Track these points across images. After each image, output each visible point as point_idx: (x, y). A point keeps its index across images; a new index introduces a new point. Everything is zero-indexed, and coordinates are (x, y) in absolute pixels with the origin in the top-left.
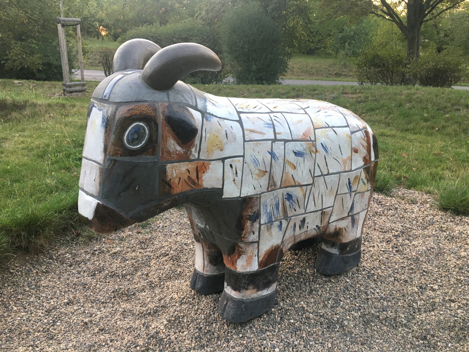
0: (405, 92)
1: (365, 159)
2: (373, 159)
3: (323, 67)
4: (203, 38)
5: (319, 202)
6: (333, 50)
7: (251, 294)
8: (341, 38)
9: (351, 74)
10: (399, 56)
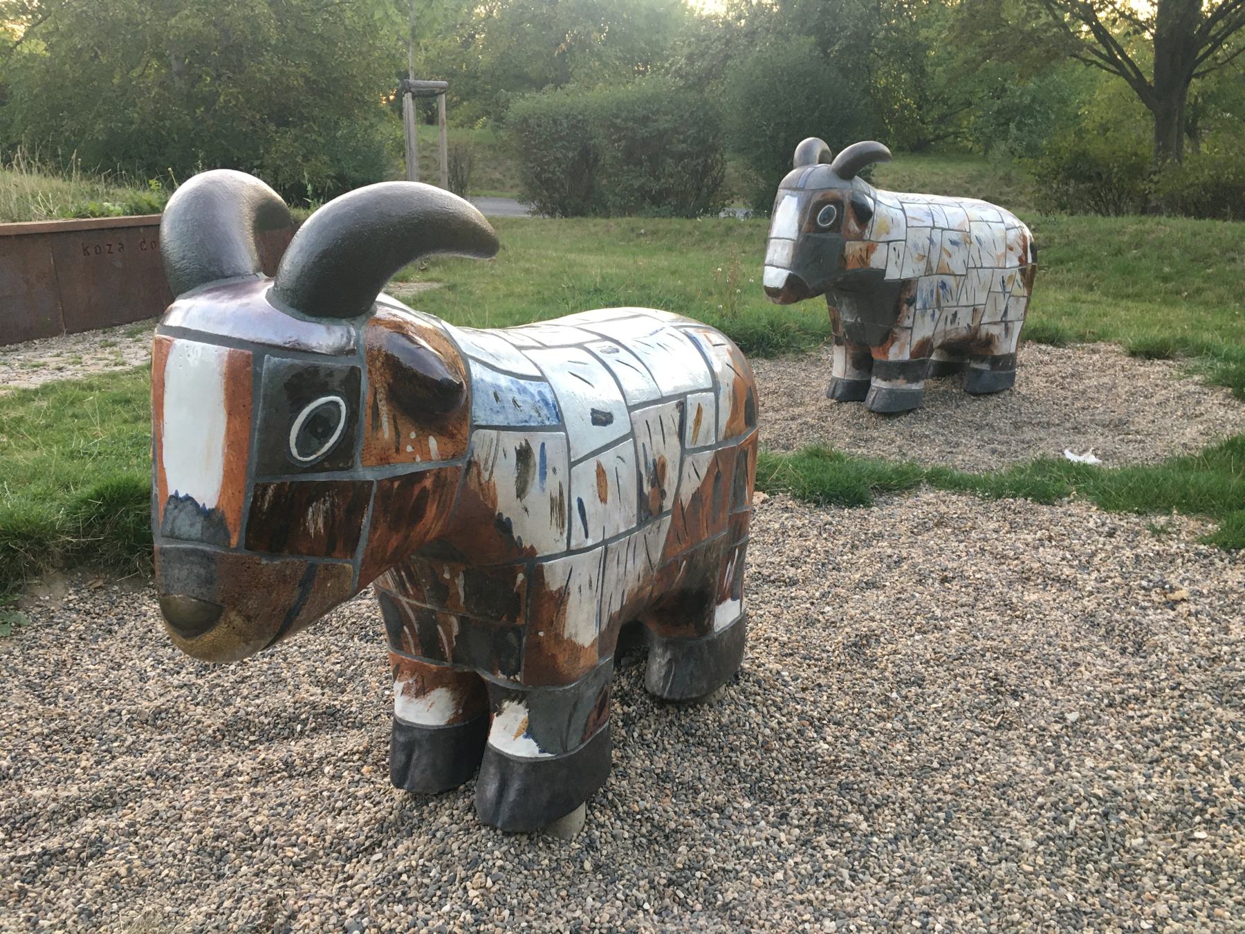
0: (1132, 228)
1: (1020, 259)
2: (1030, 261)
3: (952, 183)
4: (681, 117)
5: (971, 297)
6: (977, 141)
7: (901, 385)
8: (999, 112)
9: (1022, 199)
10: (1136, 154)
